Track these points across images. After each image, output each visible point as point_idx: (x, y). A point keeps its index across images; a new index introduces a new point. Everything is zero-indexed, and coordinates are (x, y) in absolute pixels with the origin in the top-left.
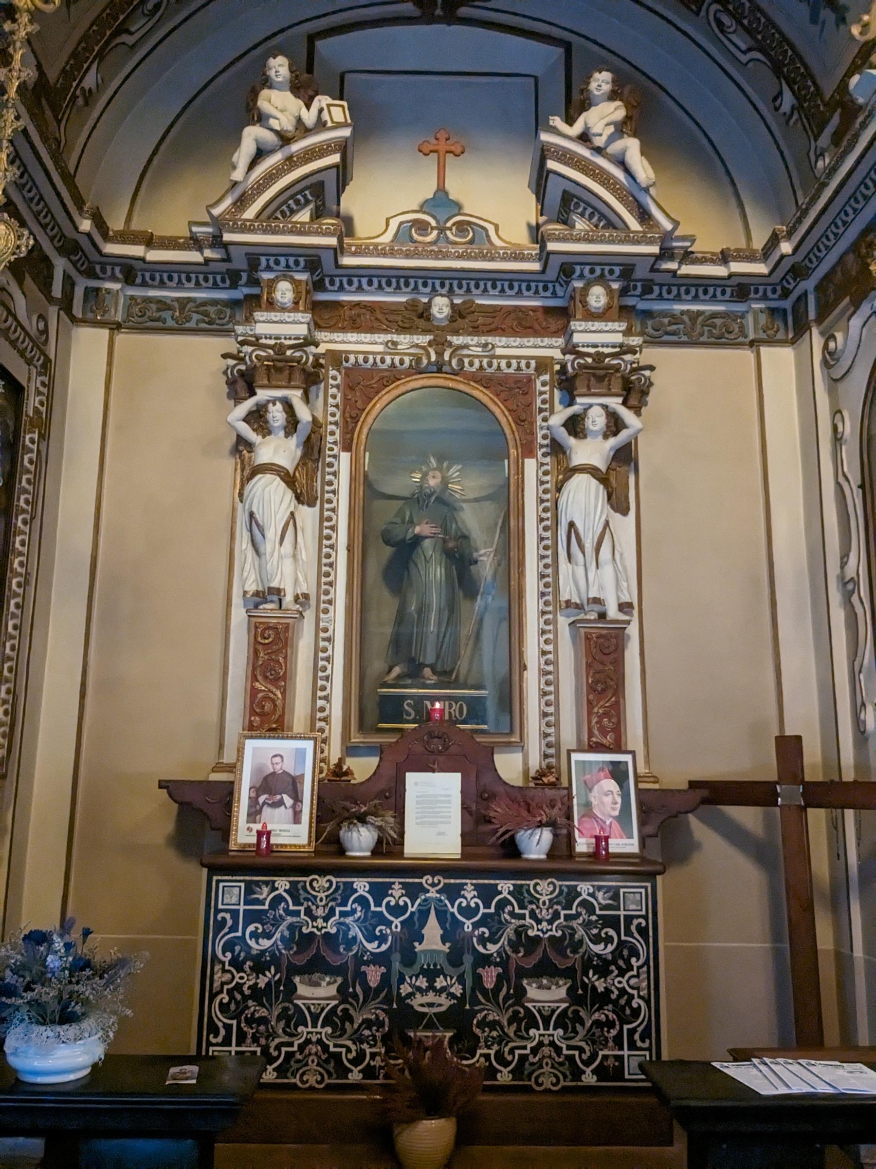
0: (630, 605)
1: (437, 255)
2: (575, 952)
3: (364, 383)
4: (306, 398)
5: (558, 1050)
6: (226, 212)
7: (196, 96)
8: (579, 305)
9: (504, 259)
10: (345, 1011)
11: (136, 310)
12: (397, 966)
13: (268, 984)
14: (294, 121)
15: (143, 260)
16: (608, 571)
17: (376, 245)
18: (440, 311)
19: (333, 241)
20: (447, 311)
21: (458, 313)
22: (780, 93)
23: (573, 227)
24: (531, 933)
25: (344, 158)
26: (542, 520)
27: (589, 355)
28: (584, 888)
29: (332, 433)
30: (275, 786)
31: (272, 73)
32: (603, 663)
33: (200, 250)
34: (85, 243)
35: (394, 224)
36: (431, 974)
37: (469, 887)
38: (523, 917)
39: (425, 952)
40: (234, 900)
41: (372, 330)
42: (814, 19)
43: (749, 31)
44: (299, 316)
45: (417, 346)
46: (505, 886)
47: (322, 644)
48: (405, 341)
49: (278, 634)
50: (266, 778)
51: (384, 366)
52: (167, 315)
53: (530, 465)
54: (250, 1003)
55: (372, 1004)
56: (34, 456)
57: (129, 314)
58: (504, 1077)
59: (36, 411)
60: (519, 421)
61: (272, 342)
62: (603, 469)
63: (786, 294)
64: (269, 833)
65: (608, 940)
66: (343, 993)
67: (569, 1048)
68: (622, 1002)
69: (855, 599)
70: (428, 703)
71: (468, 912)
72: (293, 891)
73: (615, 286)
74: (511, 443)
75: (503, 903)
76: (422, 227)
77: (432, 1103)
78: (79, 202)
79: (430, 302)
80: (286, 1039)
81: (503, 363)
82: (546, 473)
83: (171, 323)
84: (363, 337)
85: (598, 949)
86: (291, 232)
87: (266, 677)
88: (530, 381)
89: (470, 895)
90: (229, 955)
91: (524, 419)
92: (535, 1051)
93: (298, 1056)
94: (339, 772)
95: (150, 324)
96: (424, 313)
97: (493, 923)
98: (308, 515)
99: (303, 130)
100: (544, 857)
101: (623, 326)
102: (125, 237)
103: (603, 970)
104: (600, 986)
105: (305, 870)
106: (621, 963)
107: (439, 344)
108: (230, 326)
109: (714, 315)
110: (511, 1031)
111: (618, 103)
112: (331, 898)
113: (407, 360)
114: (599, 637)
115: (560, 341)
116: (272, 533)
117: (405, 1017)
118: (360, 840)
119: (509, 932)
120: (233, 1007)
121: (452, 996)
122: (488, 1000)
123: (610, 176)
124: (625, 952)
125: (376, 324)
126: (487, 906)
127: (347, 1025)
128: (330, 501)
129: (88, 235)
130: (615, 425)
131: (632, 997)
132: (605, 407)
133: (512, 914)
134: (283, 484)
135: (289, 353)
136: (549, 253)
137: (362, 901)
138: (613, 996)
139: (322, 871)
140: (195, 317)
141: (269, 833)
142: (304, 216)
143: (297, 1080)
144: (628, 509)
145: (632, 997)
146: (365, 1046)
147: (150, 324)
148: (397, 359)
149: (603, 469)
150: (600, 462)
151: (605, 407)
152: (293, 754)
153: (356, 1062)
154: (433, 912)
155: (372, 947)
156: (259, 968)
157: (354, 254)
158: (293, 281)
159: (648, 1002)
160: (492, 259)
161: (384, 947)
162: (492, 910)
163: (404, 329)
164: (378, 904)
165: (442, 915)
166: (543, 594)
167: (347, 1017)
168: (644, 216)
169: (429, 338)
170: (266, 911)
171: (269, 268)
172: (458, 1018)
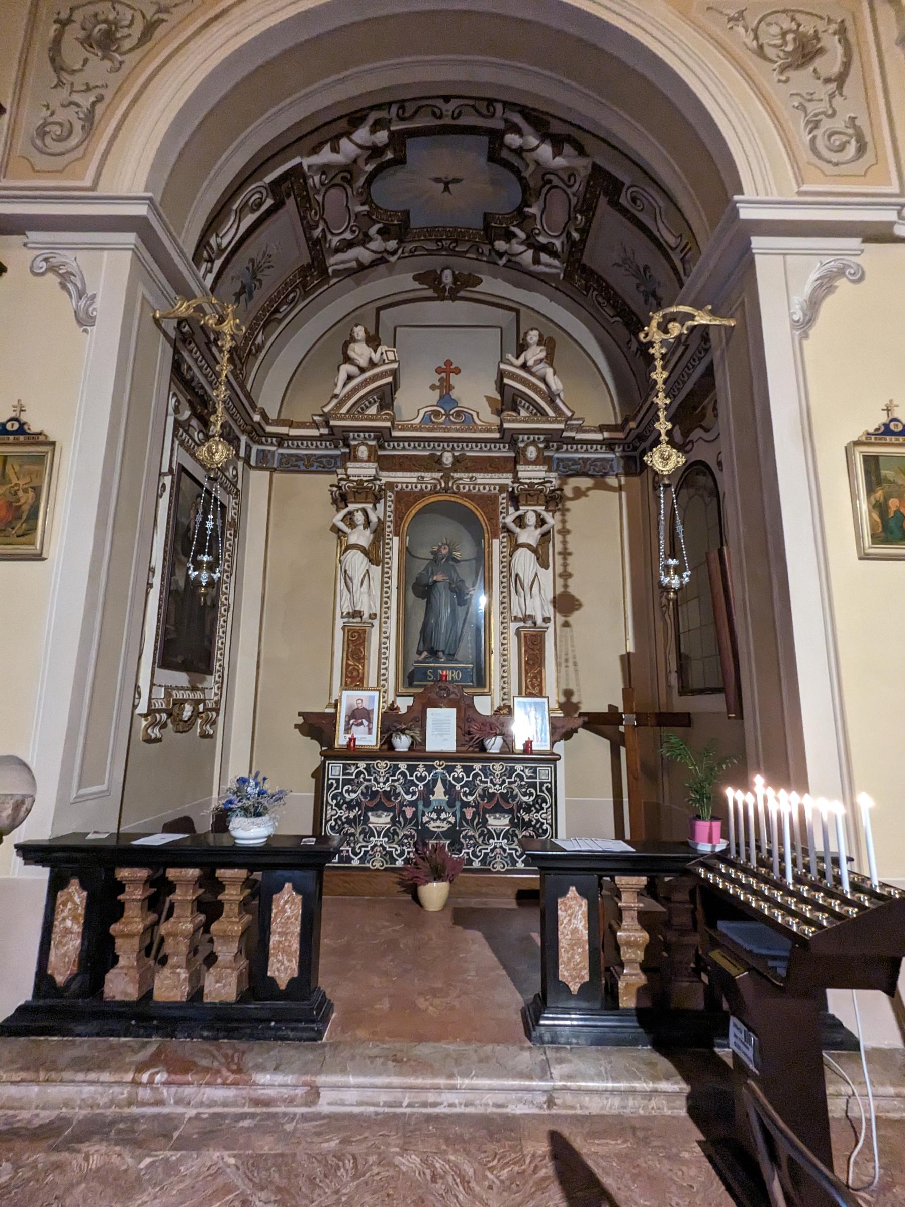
0: (549, 618)
1: (445, 430)
2: (513, 800)
3: (405, 499)
4: (375, 508)
5: (504, 851)
6: (332, 409)
7: (316, 343)
8: (522, 456)
9: (481, 431)
10: (394, 830)
11: (283, 460)
12: (421, 807)
13: (355, 816)
14: (367, 360)
15: (288, 435)
16: (537, 600)
17: (412, 425)
18: (447, 459)
19: (388, 424)
20: (451, 460)
21: (456, 460)
22: (631, 341)
23: (519, 414)
24: (490, 791)
25: (395, 379)
26: (502, 572)
27: (526, 484)
28: (519, 767)
29: (389, 527)
30: (358, 715)
31: (356, 335)
32: (533, 650)
33: (318, 429)
34: (257, 427)
35: (422, 413)
36: (439, 811)
37: (459, 767)
38: (486, 782)
39: (436, 800)
40: (338, 773)
41: (411, 470)
42: (646, 301)
43: (614, 307)
44: (371, 464)
45: (434, 479)
46: (477, 767)
47: (384, 640)
48: (428, 476)
49: (360, 634)
50: (354, 711)
51: (417, 490)
52: (300, 463)
53: (496, 543)
54: (346, 826)
55: (408, 827)
56: (231, 542)
57: (280, 463)
58: (476, 864)
59: (233, 518)
60: (489, 519)
61: (356, 479)
62: (535, 546)
63: (635, 449)
64: (355, 739)
65: (531, 794)
66: (393, 821)
67: (510, 849)
68: (538, 826)
69: (666, 615)
70: (440, 672)
71: (458, 780)
72: (367, 769)
73: (541, 445)
74: (485, 531)
75: (477, 775)
76: (437, 414)
77: (438, 875)
78: (254, 406)
79: (441, 455)
80: (364, 844)
81: (481, 487)
82: (504, 547)
83: (303, 468)
84: (405, 474)
85: (525, 799)
86: (366, 420)
87: (353, 658)
88: (496, 497)
89: (459, 771)
90: (335, 801)
91: (492, 517)
92: (492, 851)
93: (370, 853)
94: (393, 708)
95: (291, 468)
96: (439, 460)
97: (472, 786)
98: (376, 571)
99: (372, 364)
100: (407, 750)
101: (546, 468)
102: (279, 422)
103: (528, 810)
104: (527, 818)
105: (373, 758)
106: (537, 806)
107: (447, 478)
108: (334, 469)
109: (597, 460)
110: (480, 841)
111: (542, 347)
112: (387, 772)
113: (429, 486)
114: (532, 635)
115: (510, 475)
116: (357, 581)
117: (425, 833)
118: (402, 743)
119: (479, 790)
120: (337, 827)
121: (450, 823)
122: (467, 824)
123: (537, 387)
124: (540, 801)
125: (413, 467)
126: (468, 776)
127: (396, 837)
128: (388, 563)
129: (259, 424)
130: (541, 522)
131: (543, 824)
132: (535, 512)
133: (481, 781)
134: (362, 555)
135: (365, 484)
136: (505, 429)
137: (403, 774)
138: (533, 823)
139: (383, 758)
140: (316, 464)
141: (355, 739)
142: (373, 410)
143: (370, 865)
144: (548, 566)
145: (543, 824)
146: (404, 848)
147: (291, 468)
148: (424, 486)
149: (535, 546)
150: (533, 542)
151: (535, 512)
152: (368, 698)
153: (400, 856)
154: (440, 780)
155: (408, 797)
156: (350, 807)
157: (400, 430)
158: (367, 445)
159: (551, 826)
160: (475, 432)
161: (414, 798)
162: (470, 779)
163: (427, 470)
164: (411, 776)
165: (444, 781)
166: (502, 613)
167: (395, 833)
168: (556, 409)
169: (441, 474)
170: (353, 780)
171: (354, 439)
172: (452, 834)
